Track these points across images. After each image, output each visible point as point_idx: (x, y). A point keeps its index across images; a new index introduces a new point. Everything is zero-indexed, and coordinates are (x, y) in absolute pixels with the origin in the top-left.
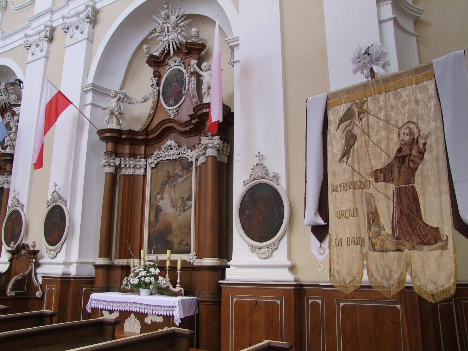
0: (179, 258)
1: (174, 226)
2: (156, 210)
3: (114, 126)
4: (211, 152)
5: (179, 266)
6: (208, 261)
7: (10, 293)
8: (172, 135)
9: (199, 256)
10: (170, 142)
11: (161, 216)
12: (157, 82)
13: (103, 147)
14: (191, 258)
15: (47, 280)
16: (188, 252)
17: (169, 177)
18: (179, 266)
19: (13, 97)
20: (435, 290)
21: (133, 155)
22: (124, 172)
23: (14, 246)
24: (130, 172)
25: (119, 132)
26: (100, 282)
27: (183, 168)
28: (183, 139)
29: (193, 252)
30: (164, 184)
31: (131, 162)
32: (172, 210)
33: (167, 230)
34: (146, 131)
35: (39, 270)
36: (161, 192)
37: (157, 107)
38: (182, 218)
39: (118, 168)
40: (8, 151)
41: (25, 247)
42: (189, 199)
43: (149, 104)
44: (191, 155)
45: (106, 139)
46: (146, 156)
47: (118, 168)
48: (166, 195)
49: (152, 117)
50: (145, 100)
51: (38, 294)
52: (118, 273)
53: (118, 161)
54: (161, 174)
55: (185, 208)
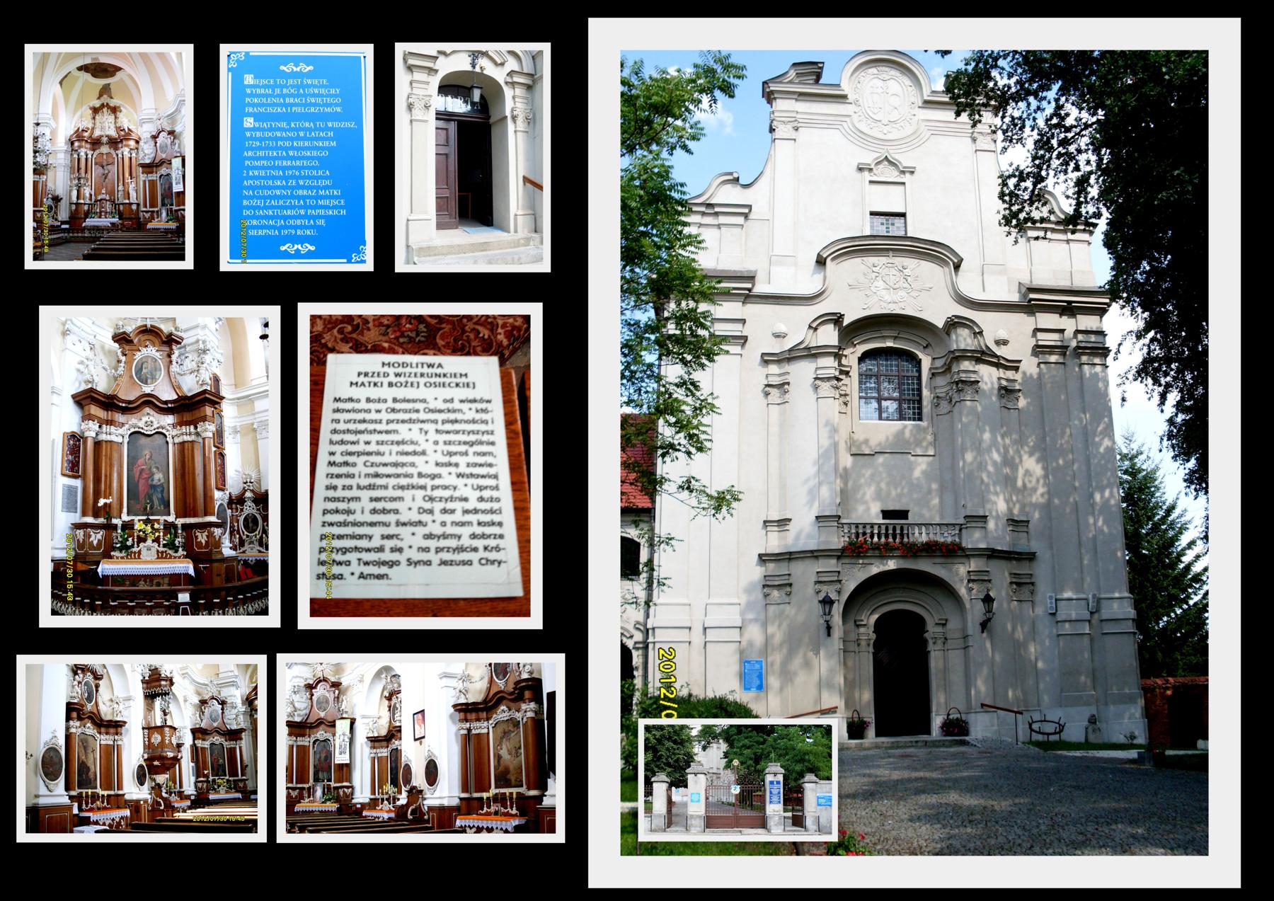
0: (514, 790)
1: (511, 768)
2: (498, 757)
3: (463, 700)
4: (530, 714)
5: (514, 796)
6: (533, 793)
7: (410, 817)
8: (504, 702)
9: (529, 789)
10: (503, 707)
11: (502, 762)
12: (926, 635)
13: (458, 716)
14: (522, 790)
15: (431, 809)
16: (522, 786)
17: (505, 733)
18: (514, 796)
19: (396, 685)
20: (862, 79)
21: (478, 720)
22: (474, 732)
23: (408, 787)
24: (477, 732)
25: (466, 704)
26: (464, 810)
27: (514, 726)
28: (511, 704)
29: (525, 786)
30: (502, 738)
31: (478, 724)
32: (509, 757)
33: (507, 771)
34: (485, 701)
35: (425, 802)
36: (500, 744)
37: (491, 681)
38: (516, 762)
39: (469, 730)
40: (398, 724)
41: (414, 788)
42: (520, 748)
43: (486, 680)
44: (518, 716)
45: (460, 711)
46: (488, 719)
47: (469, 730)
48: (504, 746)
49: (489, 689)
50: (482, 679)
51: (426, 817)
52: (475, 804)
53: (468, 725)
54: (500, 729)
55: (517, 755)
